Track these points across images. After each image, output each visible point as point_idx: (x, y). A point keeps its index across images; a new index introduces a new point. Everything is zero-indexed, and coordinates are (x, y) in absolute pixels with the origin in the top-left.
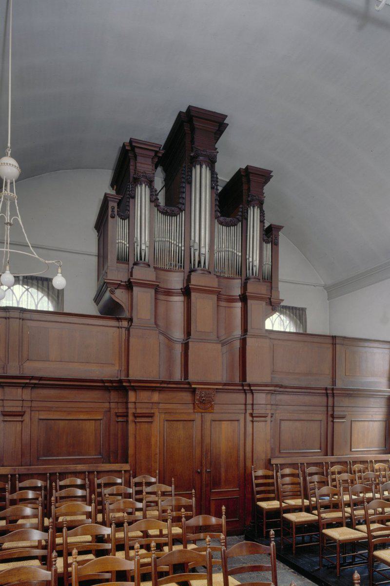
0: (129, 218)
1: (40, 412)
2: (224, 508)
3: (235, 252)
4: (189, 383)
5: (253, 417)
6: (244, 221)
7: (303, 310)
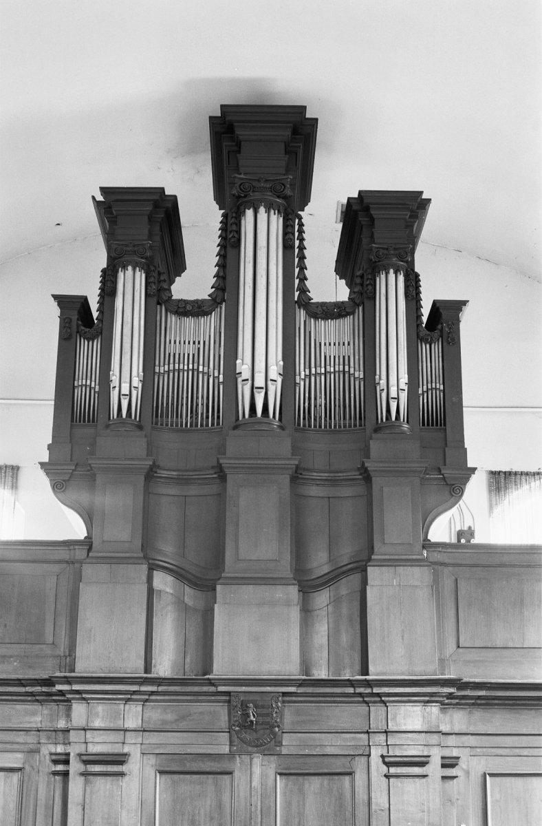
0: (101, 333)
4: (211, 683)
5: (388, 764)
6: (367, 303)
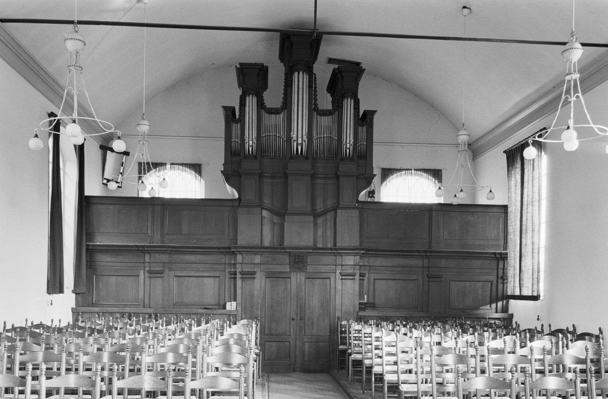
1: (175, 271)
2: (366, 296)
3: (333, 136)
7: (200, 165)
